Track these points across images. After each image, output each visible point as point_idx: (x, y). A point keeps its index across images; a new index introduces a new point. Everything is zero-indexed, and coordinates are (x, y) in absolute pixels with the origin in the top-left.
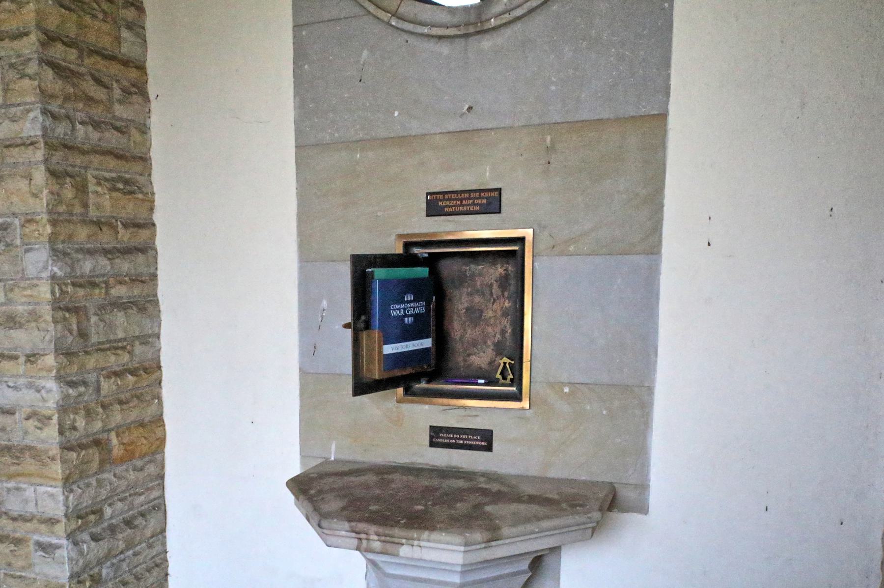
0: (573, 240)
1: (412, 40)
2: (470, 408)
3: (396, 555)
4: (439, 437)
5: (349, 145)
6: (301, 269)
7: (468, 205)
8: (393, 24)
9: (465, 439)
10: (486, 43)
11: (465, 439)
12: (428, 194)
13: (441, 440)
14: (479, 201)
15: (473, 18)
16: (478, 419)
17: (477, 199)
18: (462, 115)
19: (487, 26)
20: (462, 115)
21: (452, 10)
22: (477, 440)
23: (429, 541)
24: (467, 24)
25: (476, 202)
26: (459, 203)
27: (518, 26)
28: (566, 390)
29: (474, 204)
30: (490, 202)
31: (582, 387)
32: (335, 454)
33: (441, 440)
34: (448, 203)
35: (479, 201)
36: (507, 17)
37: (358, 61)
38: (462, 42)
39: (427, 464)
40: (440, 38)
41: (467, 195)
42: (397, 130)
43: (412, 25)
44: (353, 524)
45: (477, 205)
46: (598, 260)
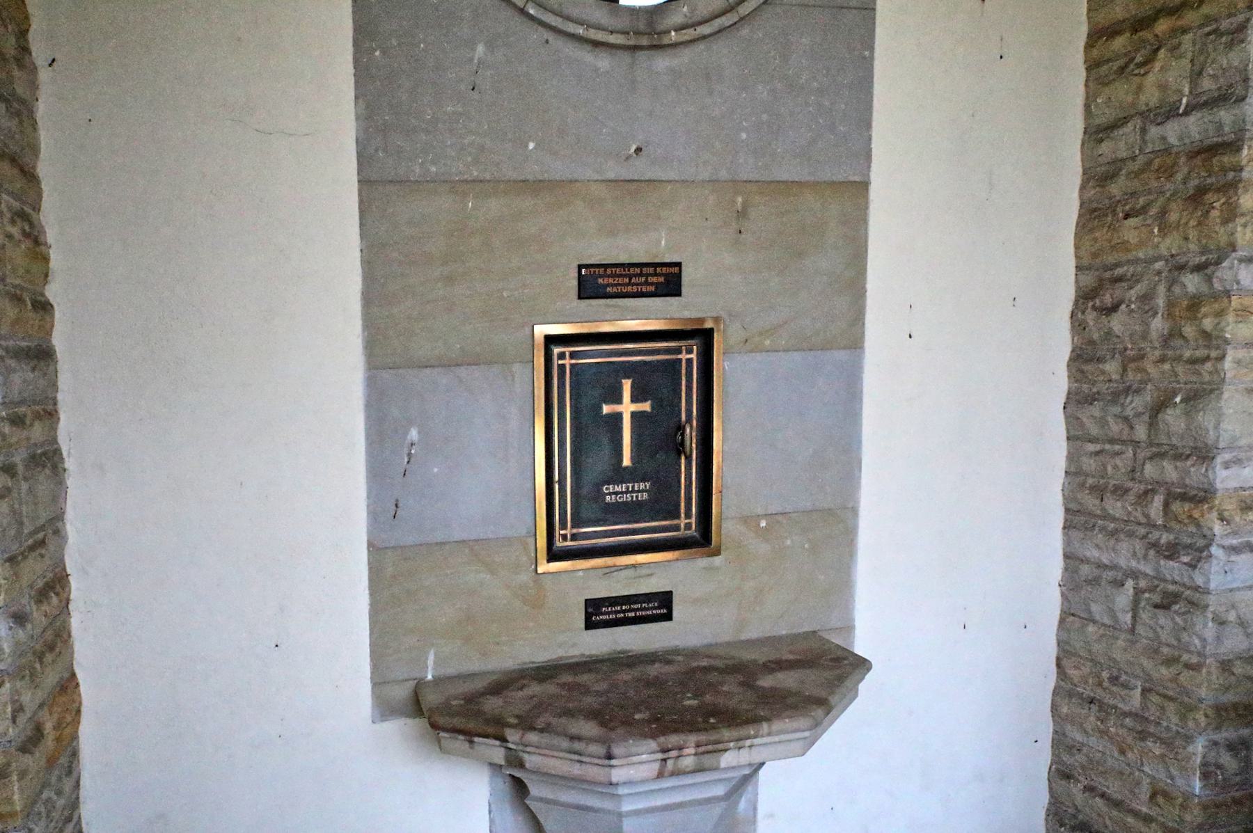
0: (773, 330)
1: (557, 42)
2: (641, 565)
3: (717, 769)
4: (598, 613)
5: (460, 187)
6: (371, 383)
7: (638, 284)
8: (532, 12)
9: (638, 609)
10: (662, 62)
11: (638, 609)
12: (580, 267)
13: (604, 617)
14: (654, 279)
15: (642, 26)
16: (653, 580)
17: (652, 275)
18: (628, 158)
19: (666, 41)
20: (628, 158)
21: (633, 11)
22: (655, 608)
23: (769, 734)
24: (638, 33)
25: (651, 279)
26: (627, 280)
27: (701, 46)
28: (763, 524)
29: (646, 283)
30: (667, 281)
31: (780, 518)
32: (434, 669)
33: (604, 617)
34: (611, 281)
35: (654, 279)
36: (689, 34)
37: (471, 60)
38: (626, 57)
39: (583, 655)
40: (596, 44)
41: (638, 270)
42: (532, 171)
43: (560, 20)
44: (662, 739)
45: (652, 284)
46: (797, 356)
